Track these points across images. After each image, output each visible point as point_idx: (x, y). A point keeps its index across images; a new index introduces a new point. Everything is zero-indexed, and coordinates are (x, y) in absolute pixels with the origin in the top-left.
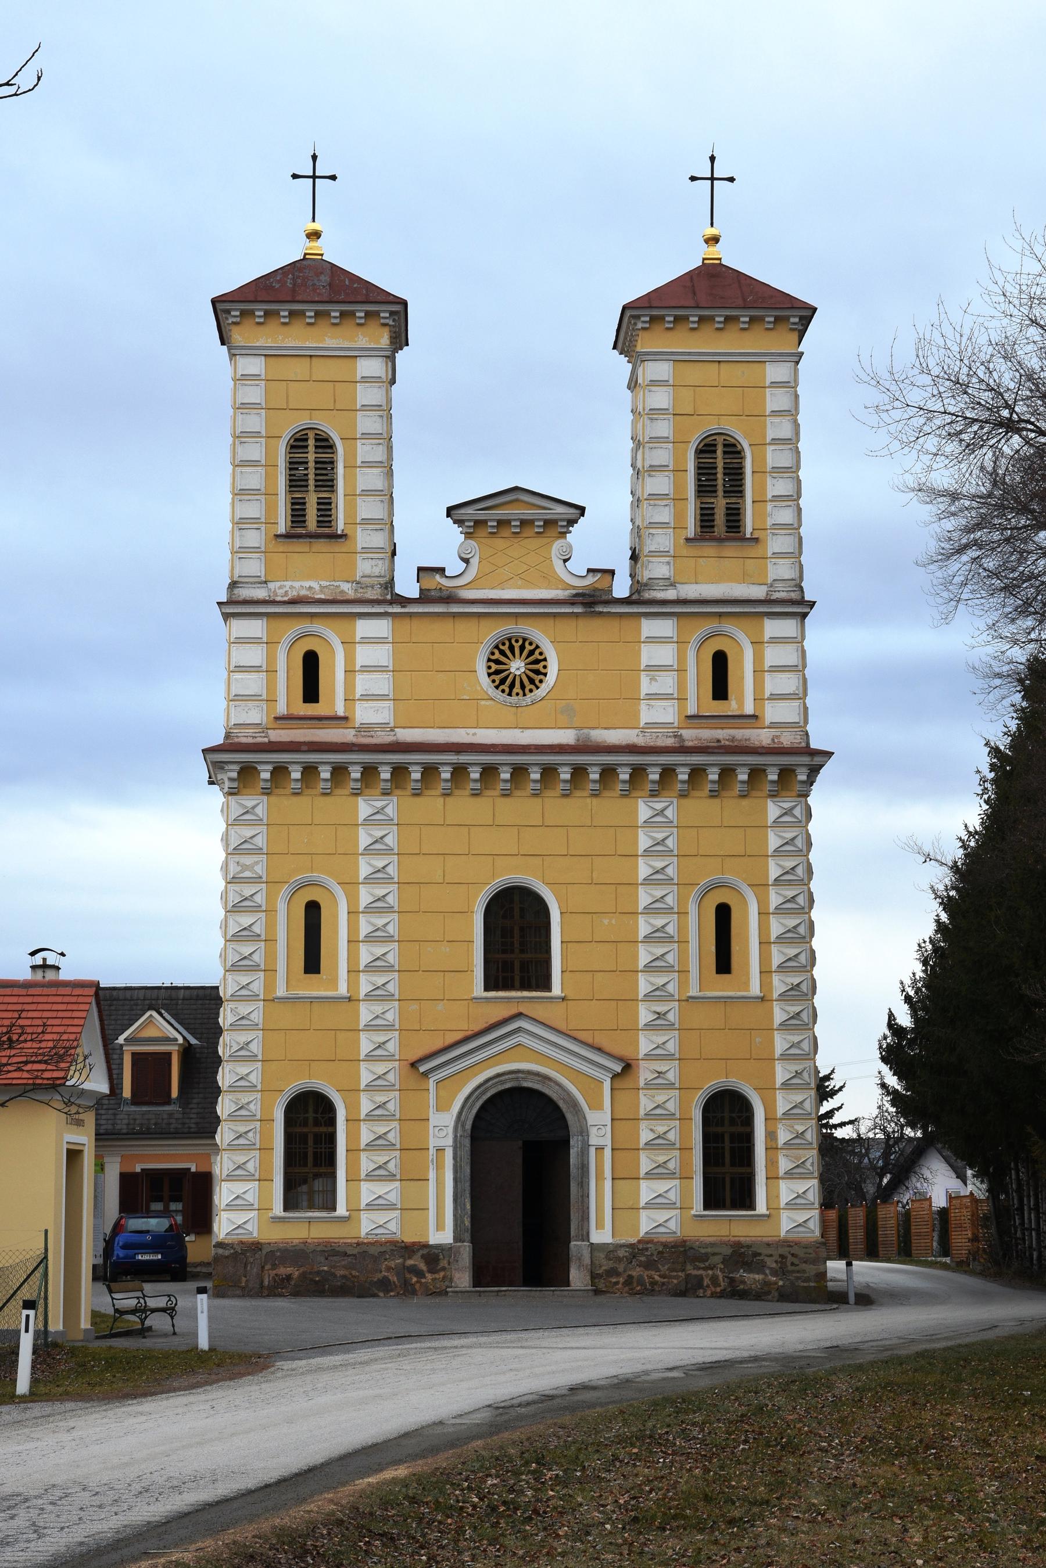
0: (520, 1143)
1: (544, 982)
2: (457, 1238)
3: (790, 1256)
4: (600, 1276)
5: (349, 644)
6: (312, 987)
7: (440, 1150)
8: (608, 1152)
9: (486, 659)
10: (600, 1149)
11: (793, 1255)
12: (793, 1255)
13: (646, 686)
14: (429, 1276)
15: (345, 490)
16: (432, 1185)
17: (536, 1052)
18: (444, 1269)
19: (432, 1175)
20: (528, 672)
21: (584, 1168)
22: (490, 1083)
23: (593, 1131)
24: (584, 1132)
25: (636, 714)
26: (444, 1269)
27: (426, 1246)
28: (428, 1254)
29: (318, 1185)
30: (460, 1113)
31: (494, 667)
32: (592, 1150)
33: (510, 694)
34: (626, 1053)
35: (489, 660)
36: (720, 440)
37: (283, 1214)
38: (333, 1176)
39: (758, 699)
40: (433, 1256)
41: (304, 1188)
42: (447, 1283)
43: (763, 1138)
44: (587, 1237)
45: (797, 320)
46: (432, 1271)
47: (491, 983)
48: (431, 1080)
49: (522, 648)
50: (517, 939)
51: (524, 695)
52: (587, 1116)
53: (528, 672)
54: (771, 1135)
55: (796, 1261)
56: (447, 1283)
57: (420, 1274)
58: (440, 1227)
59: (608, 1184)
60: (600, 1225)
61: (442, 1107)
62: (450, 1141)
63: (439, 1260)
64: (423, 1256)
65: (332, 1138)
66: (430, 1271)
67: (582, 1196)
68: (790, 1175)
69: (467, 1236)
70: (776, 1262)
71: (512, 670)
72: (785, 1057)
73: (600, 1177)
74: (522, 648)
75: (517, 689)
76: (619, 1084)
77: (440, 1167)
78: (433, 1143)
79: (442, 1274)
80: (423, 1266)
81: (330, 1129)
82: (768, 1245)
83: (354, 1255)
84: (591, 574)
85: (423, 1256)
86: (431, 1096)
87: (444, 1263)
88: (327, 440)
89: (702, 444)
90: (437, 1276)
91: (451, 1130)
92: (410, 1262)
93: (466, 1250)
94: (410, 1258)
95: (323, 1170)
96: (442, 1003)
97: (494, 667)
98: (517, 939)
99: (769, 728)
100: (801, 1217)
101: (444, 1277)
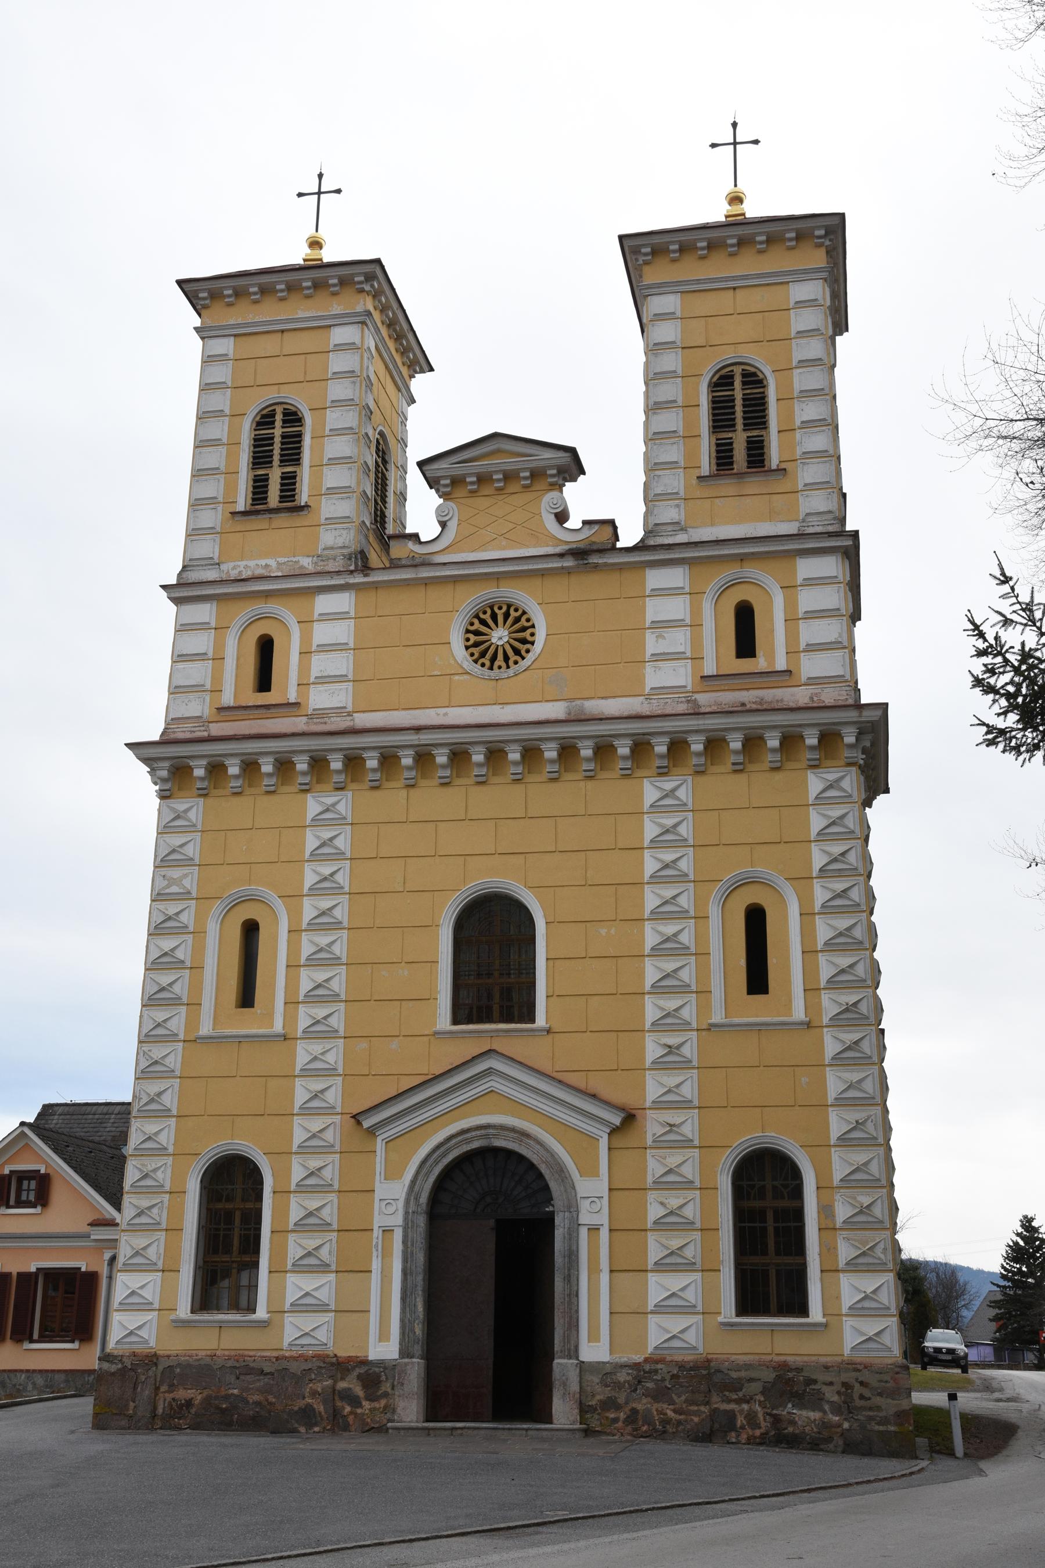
0: (492, 1223)
2: (404, 1353)
4: (593, 1409)
6: (246, 1023)
7: (387, 1231)
8: (604, 1234)
9: (462, 630)
10: (594, 1229)
11: (862, 1383)
12: (862, 1383)
16: (375, 1278)
18: (386, 1395)
19: (376, 1265)
20: (512, 641)
21: (572, 1256)
22: (454, 1141)
23: (584, 1206)
24: (572, 1207)
25: (641, 680)
26: (386, 1395)
27: (364, 1362)
30: (413, 1182)
32: (583, 1232)
35: (468, 631)
36: (738, 370)
38: (256, 1265)
39: (792, 652)
40: (374, 1377)
41: (225, 1283)
42: (389, 1415)
44: (573, 1352)
47: (462, 1013)
48: (379, 1139)
49: (507, 615)
50: (492, 960)
53: (512, 641)
54: (826, 1210)
55: (867, 1393)
56: (389, 1415)
57: (355, 1402)
58: (383, 1336)
59: (605, 1278)
60: (594, 1337)
61: (391, 1175)
62: (398, 1220)
63: (380, 1382)
66: (367, 1399)
67: (569, 1295)
69: (418, 1349)
71: (494, 640)
73: (594, 1269)
75: (500, 661)
76: (618, 1142)
77: (387, 1254)
79: (383, 1402)
80: (359, 1391)
82: (827, 1367)
84: (587, 527)
87: (386, 1387)
90: (376, 1405)
91: (401, 1204)
92: (342, 1385)
93: (415, 1370)
94: (343, 1379)
96: (396, 1039)
97: (473, 638)
98: (492, 960)
100: (871, 1327)
101: (386, 1407)
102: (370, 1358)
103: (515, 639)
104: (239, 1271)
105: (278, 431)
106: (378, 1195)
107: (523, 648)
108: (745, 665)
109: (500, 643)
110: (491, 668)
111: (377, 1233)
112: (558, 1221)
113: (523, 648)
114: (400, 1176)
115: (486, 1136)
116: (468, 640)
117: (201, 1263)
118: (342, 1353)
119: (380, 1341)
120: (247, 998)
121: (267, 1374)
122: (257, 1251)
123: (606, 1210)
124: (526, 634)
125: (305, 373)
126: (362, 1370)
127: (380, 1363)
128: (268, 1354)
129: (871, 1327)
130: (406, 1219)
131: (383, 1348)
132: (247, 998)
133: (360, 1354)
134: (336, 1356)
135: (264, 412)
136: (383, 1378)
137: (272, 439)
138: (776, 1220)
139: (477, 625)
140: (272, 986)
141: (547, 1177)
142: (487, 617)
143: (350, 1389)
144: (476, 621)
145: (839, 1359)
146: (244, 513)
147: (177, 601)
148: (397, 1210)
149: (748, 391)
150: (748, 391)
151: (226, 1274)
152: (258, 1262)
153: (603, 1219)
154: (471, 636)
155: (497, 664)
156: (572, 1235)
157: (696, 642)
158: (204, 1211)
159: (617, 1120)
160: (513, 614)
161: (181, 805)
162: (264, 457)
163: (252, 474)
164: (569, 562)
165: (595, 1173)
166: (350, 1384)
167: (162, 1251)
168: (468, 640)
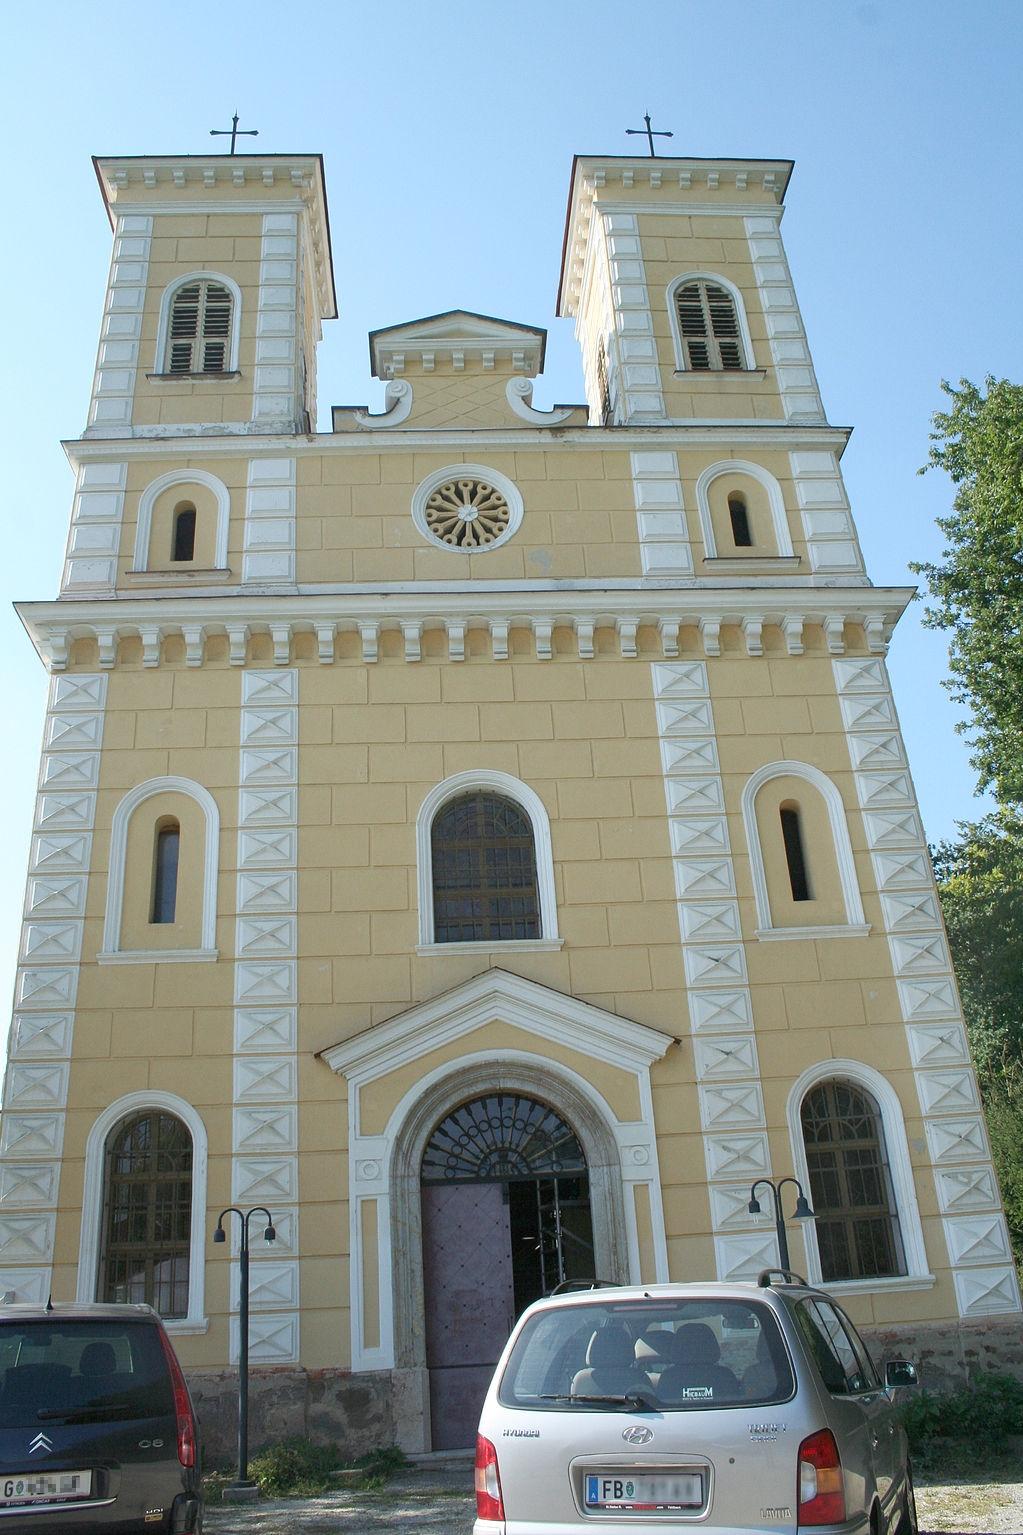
1: (528, 925)
2: (403, 1356)
3: (982, 1352)
5: (236, 490)
6: (161, 949)
9: (423, 507)
11: (987, 1349)
12: (987, 1349)
13: (644, 525)
14: (352, 1434)
15: (241, 333)
17: (518, 1015)
18: (378, 1418)
20: (482, 519)
21: (617, 1222)
23: (627, 1157)
24: (613, 1161)
25: (636, 561)
26: (378, 1418)
27: (346, 1375)
28: (351, 1392)
29: (163, 1271)
30: (399, 1140)
31: (436, 514)
33: (459, 544)
34: (678, 1033)
35: (429, 507)
36: (702, 286)
37: (104, 1310)
38: (185, 1254)
39: (797, 540)
40: (361, 1395)
41: (140, 1277)
43: (905, 1151)
45: (771, 178)
46: (358, 1423)
47: (445, 930)
49: (473, 494)
50: (483, 870)
51: (478, 544)
52: (616, 1132)
53: (482, 519)
54: (917, 1146)
55: (994, 1359)
57: (335, 1429)
58: (371, 1340)
62: (384, 1185)
64: (340, 1396)
65: (186, 1189)
66: (351, 1425)
68: (958, 1211)
70: (961, 1364)
71: (461, 516)
72: (683, 817)
74: (473, 494)
75: (469, 537)
78: (355, 1191)
80: (340, 1414)
81: (183, 1175)
82: (943, 1334)
83: (217, 1399)
84: (559, 411)
85: (340, 1396)
86: (351, 1109)
87: (377, 1407)
88: (222, 290)
89: (682, 289)
92: (317, 1408)
94: (316, 1400)
95: (168, 1245)
97: (436, 514)
98: (483, 870)
99: (816, 573)
100: (993, 1278)
102: (353, 1370)
103: (485, 517)
104: (156, 1262)
105: (202, 305)
106: (352, 1156)
107: (494, 526)
108: (743, 550)
109: (469, 519)
110: (459, 544)
111: (354, 1206)
112: (592, 1178)
113: (494, 526)
114: (380, 1130)
115: (494, 1077)
116: (430, 515)
117: (104, 1252)
118: (314, 1366)
119: (366, 1347)
120: (161, 909)
121: (210, 1399)
122: (185, 1234)
123: (654, 1160)
124: (498, 513)
125: (234, 254)
126: (344, 1386)
127: (370, 1377)
128: (208, 1372)
129: (993, 1278)
130: (393, 1185)
131: (373, 1355)
132: (161, 909)
133: (340, 1365)
134: (304, 1370)
135: (187, 287)
136: (373, 1394)
137: (196, 311)
138: (865, 1171)
139: (439, 501)
140: (198, 896)
141: (577, 1124)
142: (451, 494)
143: (327, 1414)
144: (439, 497)
145: (953, 1321)
146: (163, 376)
147: (84, 461)
148: (380, 1173)
149: (715, 304)
150: (715, 304)
151: (139, 1264)
152: (188, 1249)
153: (652, 1173)
154: (433, 511)
155: (465, 541)
156: (614, 1197)
157: (692, 526)
158: (108, 1185)
159: (661, 1046)
160: (481, 492)
161: (80, 679)
162: (192, 333)
163: (172, 342)
164: (546, 438)
165: (633, 1116)
166: (328, 1406)
167: (52, 1238)
168: (430, 515)
